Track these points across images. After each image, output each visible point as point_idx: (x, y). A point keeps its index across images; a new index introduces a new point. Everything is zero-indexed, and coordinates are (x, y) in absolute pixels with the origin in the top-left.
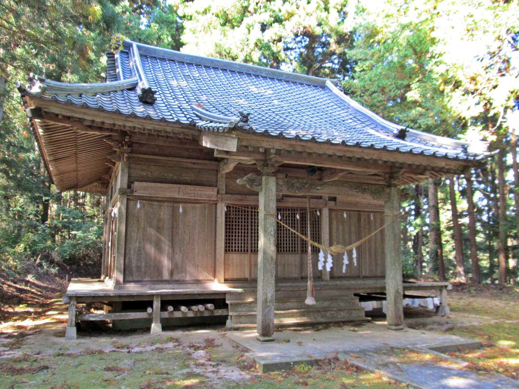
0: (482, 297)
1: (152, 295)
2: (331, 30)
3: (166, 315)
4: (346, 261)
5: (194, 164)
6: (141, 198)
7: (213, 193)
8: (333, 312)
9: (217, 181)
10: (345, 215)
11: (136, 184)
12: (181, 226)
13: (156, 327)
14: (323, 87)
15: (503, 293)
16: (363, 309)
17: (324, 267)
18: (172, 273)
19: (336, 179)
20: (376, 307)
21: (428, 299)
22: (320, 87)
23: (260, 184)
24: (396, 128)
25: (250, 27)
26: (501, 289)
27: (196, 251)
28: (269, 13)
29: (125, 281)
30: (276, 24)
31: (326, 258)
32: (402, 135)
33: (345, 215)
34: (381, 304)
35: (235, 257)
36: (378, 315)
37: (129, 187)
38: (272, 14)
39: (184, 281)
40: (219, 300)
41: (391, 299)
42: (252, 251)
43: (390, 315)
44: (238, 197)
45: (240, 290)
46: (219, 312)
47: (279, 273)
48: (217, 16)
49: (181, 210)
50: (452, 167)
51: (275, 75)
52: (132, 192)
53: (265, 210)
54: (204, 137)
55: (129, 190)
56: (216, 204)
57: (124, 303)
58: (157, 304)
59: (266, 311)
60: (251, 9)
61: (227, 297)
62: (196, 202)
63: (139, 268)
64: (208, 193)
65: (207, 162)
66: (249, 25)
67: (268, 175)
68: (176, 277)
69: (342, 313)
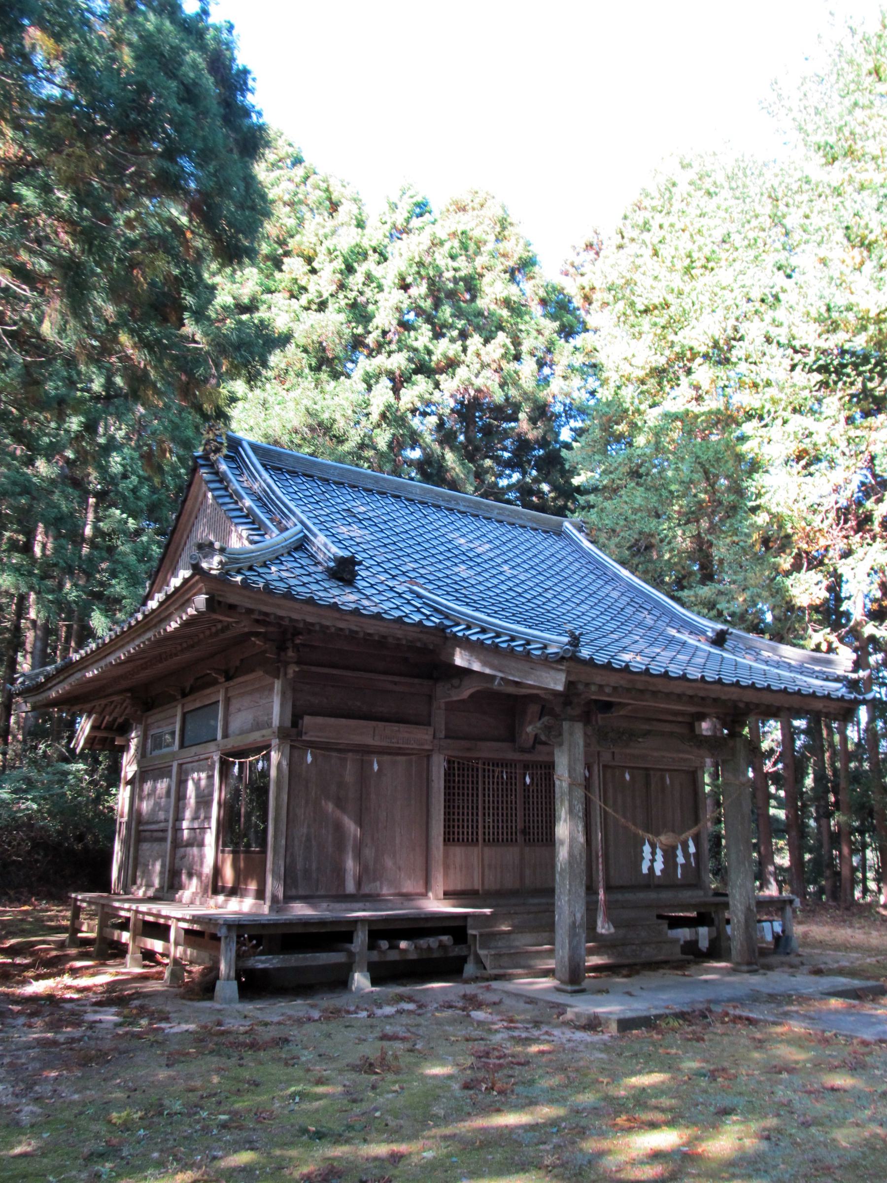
0: (817, 924)
1: (356, 921)
2: (526, 396)
3: (375, 956)
4: (681, 860)
5: (395, 683)
6: (312, 745)
7: (426, 737)
8: (634, 947)
9: (430, 716)
10: (627, 777)
11: (307, 720)
12: (373, 796)
13: (361, 980)
14: (559, 533)
15: (854, 915)
16: (678, 940)
17: (651, 869)
18: (359, 884)
19: (621, 713)
20: (688, 938)
21: (764, 924)
22: (555, 534)
23: (560, 734)
24: (712, 627)
25: (371, 377)
26: (847, 909)
27: (397, 841)
28: (405, 354)
29: (288, 898)
30: (419, 378)
31: (653, 853)
32: (719, 640)
33: (627, 777)
34: (697, 933)
35: (458, 852)
36: (716, 951)
37: (295, 724)
38: (412, 355)
39: (378, 895)
40: (456, 928)
41: (738, 921)
42: (484, 840)
43: (739, 947)
44: (463, 742)
45: (487, 911)
46: (457, 951)
47: (486, 882)
48: (305, 351)
49: (376, 767)
50: (832, 711)
51: (481, 509)
52: (300, 734)
53: (570, 777)
54: (458, 650)
55: (294, 730)
56: (429, 757)
57: (285, 936)
58: (361, 938)
59: (575, 943)
60: (370, 340)
61: (470, 922)
62: (399, 752)
63: (307, 872)
64: (417, 737)
65: (416, 681)
66: (367, 373)
67: (572, 719)
68: (366, 890)
69: (647, 949)
